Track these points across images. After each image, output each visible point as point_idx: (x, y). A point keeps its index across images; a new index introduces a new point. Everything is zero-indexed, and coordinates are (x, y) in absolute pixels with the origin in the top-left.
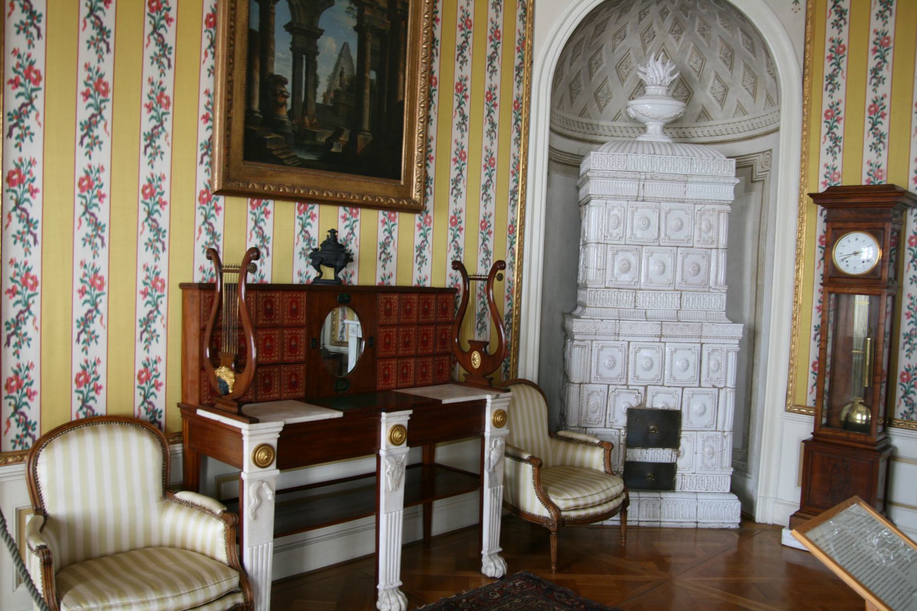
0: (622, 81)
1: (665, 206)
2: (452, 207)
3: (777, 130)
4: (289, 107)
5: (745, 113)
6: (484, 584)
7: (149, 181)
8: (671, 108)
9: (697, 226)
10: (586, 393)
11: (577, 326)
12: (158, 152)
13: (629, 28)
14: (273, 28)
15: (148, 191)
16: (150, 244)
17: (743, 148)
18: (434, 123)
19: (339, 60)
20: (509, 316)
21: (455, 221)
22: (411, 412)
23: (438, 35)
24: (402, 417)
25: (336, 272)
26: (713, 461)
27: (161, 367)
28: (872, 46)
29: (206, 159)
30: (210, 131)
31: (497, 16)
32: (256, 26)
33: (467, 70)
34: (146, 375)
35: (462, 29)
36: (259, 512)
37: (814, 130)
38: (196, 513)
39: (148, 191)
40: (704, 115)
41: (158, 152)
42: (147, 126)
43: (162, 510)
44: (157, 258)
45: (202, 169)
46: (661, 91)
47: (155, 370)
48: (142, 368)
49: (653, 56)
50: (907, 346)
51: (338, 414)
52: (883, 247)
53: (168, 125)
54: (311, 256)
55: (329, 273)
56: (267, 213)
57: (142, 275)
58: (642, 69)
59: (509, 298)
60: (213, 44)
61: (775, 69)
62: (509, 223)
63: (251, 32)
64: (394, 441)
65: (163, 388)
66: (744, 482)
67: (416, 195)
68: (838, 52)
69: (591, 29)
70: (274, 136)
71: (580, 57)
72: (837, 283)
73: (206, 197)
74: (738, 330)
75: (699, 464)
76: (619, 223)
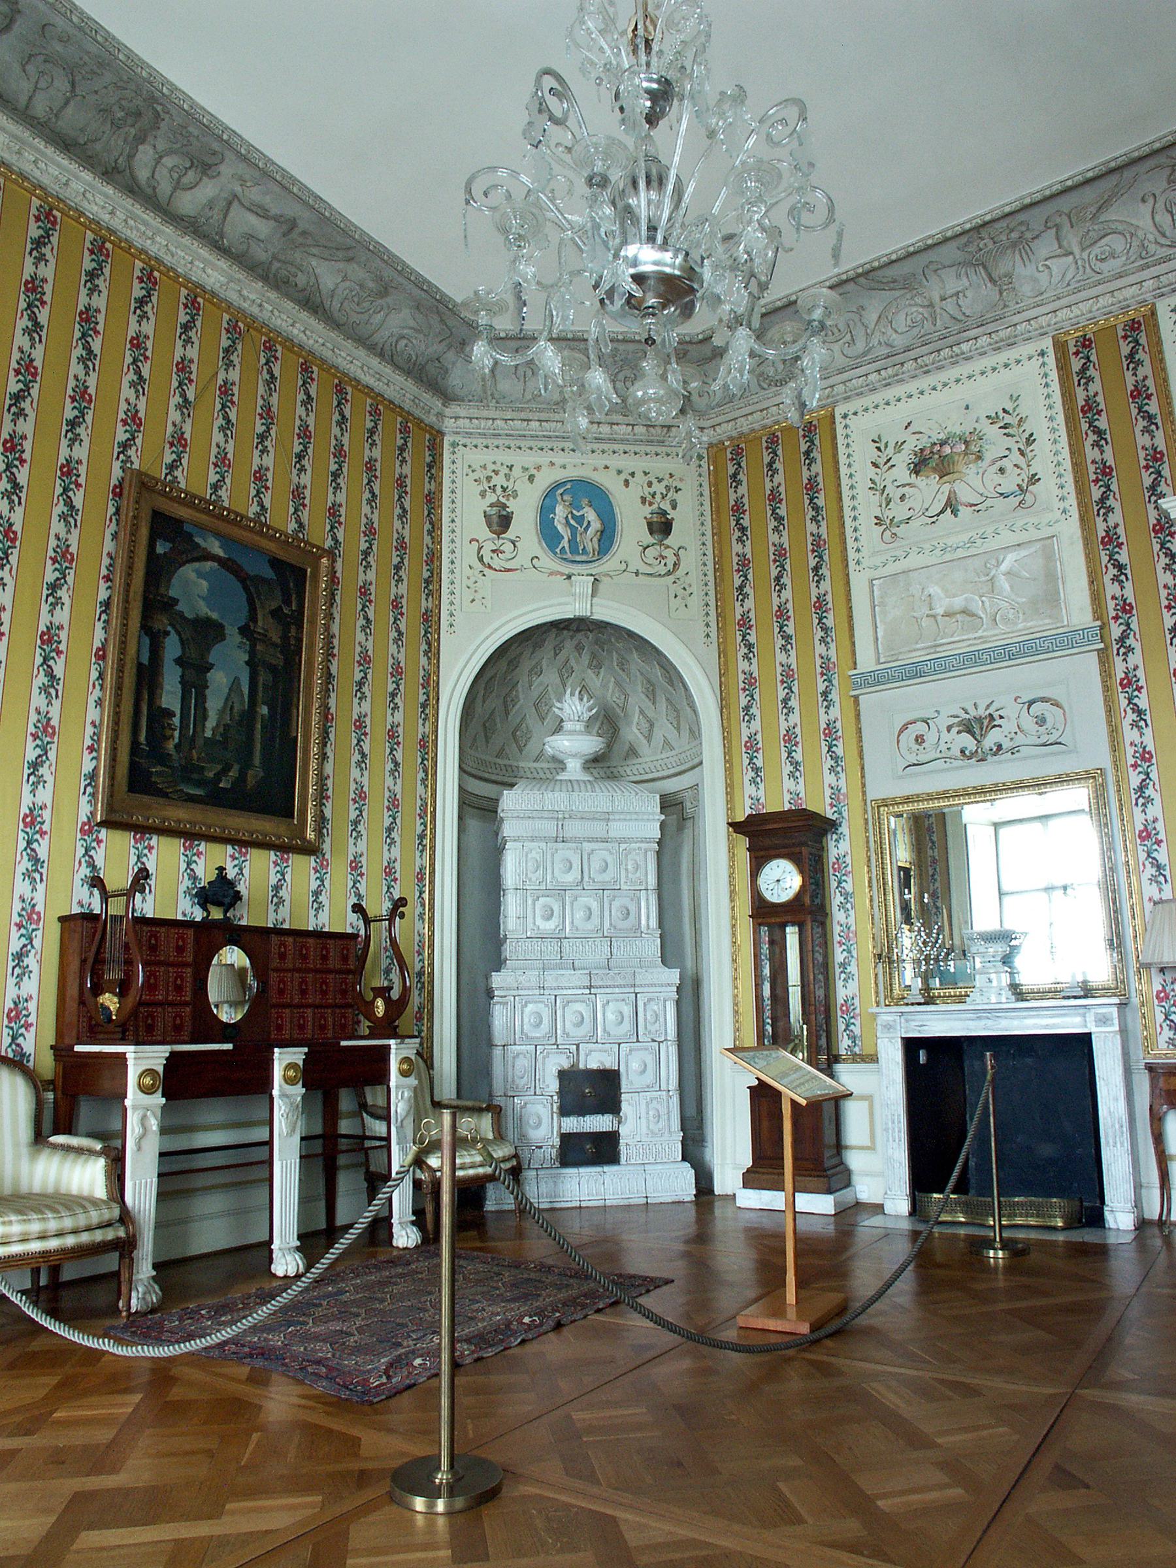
0: (542, 719)
1: (587, 846)
2: (352, 850)
3: (701, 763)
4: (177, 740)
5: (672, 749)
6: (395, 1253)
7: (30, 809)
8: (591, 744)
9: (623, 866)
10: (510, 1055)
11: (497, 980)
12: (40, 780)
13: (544, 662)
14: (162, 661)
15: (28, 820)
16: (27, 874)
17: (671, 786)
18: (331, 760)
19: (229, 694)
20: (420, 974)
21: (355, 866)
22: (306, 1050)
23: (334, 671)
24: (297, 1055)
25: (226, 912)
26: (660, 1125)
27: (32, 1006)
28: (779, 678)
29: (89, 790)
30: (94, 762)
31: (399, 652)
32: (145, 660)
33: (366, 707)
34: (16, 1014)
35: (361, 664)
36: (143, 1142)
37: (736, 760)
38: (72, 1156)
39: (28, 820)
40: (632, 752)
41: (40, 780)
42: (32, 754)
43: (33, 1157)
44: (34, 889)
45: (84, 800)
46: (579, 727)
47: (26, 1009)
48: (12, 1006)
49: (568, 692)
50: (843, 976)
51: (229, 1046)
52: (801, 872)
53: (52, 755)
54: (196, 895)
55: (217, 914)
56: (150, 848)
57: (17, 906)
58: (558, 705)
59: (419, 954)
60: (101, 676)
61: (693, 702)
62: (418, 870)
63: (140, 665)
64: (288, 1080)
65: (33, 1029)
66: (703, 1153)
67: (310, 835)
68: (751, 684)
69: (503, 664)
70: (159, 768)
71: (494, 694)
72: (766, 914)
73: (89, 828)
74: (674, 976)
75: (644, 1130)
76: (538, 867)
